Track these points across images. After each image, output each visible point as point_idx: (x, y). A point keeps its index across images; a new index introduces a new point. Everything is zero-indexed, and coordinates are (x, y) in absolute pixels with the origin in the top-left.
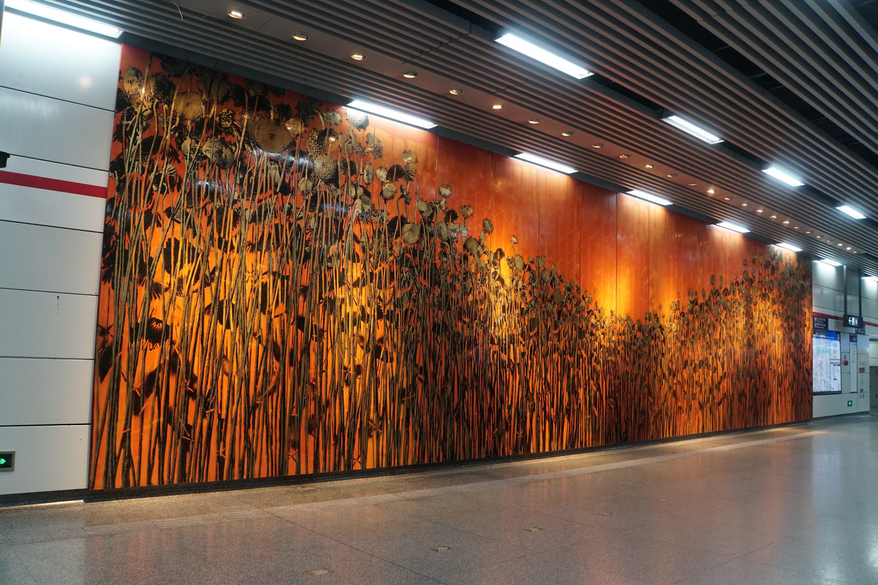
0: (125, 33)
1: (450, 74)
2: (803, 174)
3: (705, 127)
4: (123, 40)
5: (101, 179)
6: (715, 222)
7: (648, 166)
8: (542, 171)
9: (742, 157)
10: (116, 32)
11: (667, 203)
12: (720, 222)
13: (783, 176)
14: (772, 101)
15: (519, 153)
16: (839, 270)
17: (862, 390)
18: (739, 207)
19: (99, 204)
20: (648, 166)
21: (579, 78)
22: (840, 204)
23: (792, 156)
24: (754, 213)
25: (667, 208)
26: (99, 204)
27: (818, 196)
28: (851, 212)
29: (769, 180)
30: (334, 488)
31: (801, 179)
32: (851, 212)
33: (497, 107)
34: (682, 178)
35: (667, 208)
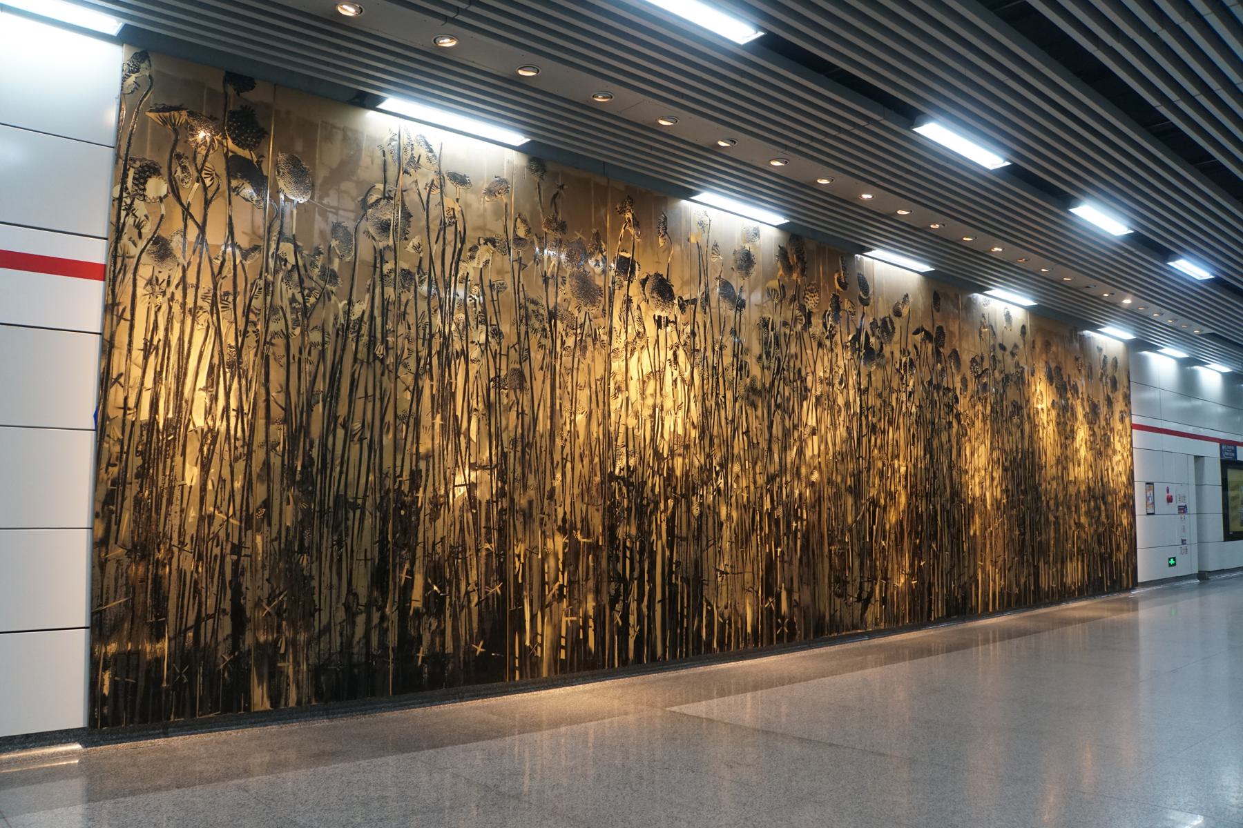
0: (126, 26)
1: (774, 137)
2: (1127, 212)
3: (954, 125)
4: (126, 37)
5: (96, 253)
6: (688, 194)
7: (996, 249)
8: (731, 219)
9: (1039, 187)
10: (113, 25)
11: (927, 268)
12: (696, 193)
13: (1102, 219)
14: (1099, 104)
15: (870, 250)
16: (1226, 376)
17: (1183, 542)
18: (892, 216)
19: (94, 290)
20: (996, 249)
21: (991, 168)
22: (1175, 257)
23: (1117, 190)
24: (926, 230)
25: (1030, 310)
26: (94, 290)
27: (1039, 187)
28: (1193, 269)
29: (1078, 226)
30: (1037, 616)
31: (1127, 222)
32: (1193, 269)
33: (866, 196)
34: (803, 168)
35: (925, 275)
